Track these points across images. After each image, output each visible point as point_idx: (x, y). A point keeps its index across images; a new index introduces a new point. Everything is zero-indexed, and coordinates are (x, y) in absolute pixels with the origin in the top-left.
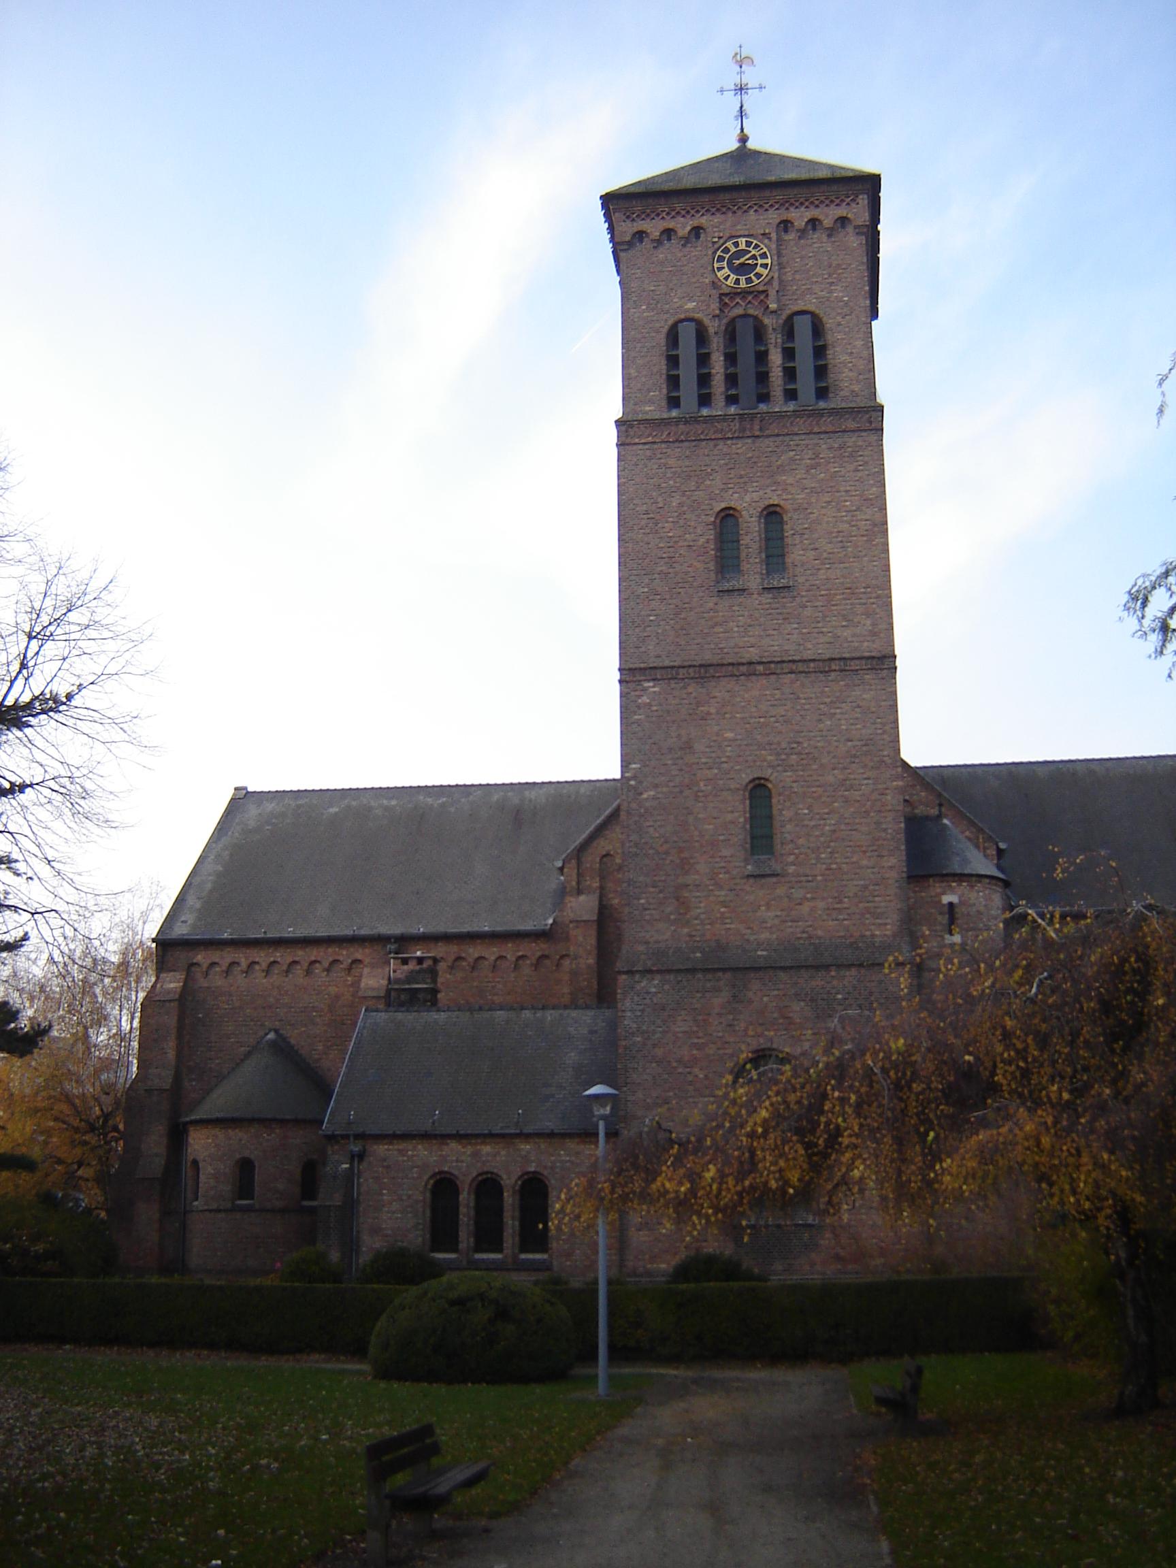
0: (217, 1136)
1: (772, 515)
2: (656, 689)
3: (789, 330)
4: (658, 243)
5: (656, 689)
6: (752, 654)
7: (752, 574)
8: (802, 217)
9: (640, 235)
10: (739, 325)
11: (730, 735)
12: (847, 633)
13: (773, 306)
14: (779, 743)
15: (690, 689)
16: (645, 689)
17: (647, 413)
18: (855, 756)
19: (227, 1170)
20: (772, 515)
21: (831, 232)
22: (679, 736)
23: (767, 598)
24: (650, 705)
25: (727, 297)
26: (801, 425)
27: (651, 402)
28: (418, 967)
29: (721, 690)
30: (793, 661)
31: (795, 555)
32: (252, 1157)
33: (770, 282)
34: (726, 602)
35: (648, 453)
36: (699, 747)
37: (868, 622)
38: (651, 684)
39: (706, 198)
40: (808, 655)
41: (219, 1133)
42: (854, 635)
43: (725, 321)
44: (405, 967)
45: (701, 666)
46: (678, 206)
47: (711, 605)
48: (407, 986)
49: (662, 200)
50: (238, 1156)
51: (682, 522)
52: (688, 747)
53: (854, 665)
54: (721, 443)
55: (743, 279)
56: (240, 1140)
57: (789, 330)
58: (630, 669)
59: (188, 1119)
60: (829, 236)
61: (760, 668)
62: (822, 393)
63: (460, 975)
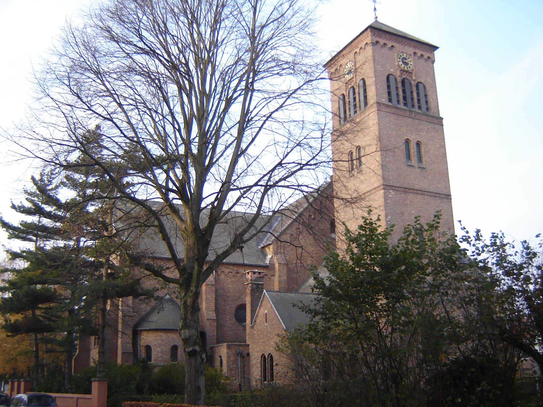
0: (162, 336)
1: (418, 144)
2: (393, 193)
3: (417, 86)
4: (382, 47)
5: (393, 193)
6: (417, 187)
7: (414, 161)
8: (419, 53)
9: (377, 42)
10: (420, 84)
11: (413, 212)
12: (439, 186)
13: (414, 78)
14: (426, 217)
15: (402, 195)
16: (390, 192)
17: (383, 101)
18: (444, 224)
19: (168, 350)
20: (418, 144)
21: (426, 60)
22: (400, 210)
23: (419, 170)
24: (392, 198)
25: (403, 71)
26: (423, 117)
27: (383, 98)
28: (259, 276)
29: (410, 196)
30: (428, 192)
31: (423, 160)
32: (178, 345)
33: (413, 70)
34: (409, 169)
35: (386, 115)
36: (406, 214)
37: (444, 184)
38: (392, 191)
39: (395, 37)
40: (431, 190)
41: (164, 335)
42: (441, 187)
43: (402, 78)
44: (255, 275)
45: (405, 188)
46: (388, 37)
47: (405, 169)
48: (256, 283)
49: (384, 33)
50: (172, 344)
51: (396, 140)
52: (403, 213)
53: (442, 196)
54: (404, 117)
55: (406, 67)
56: (173, 338)
57: (417, 86)
58: (386, 185)
59: (141, 329)
60: (425, 61)
61: (419, 192)
62: (427, 109)
63: (237, 279)
